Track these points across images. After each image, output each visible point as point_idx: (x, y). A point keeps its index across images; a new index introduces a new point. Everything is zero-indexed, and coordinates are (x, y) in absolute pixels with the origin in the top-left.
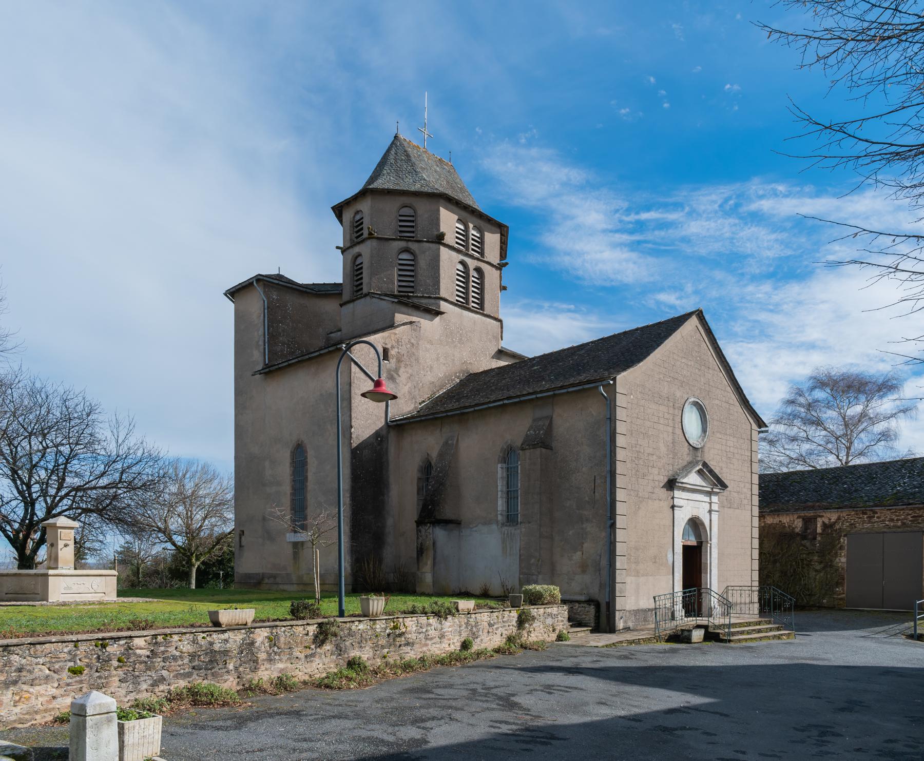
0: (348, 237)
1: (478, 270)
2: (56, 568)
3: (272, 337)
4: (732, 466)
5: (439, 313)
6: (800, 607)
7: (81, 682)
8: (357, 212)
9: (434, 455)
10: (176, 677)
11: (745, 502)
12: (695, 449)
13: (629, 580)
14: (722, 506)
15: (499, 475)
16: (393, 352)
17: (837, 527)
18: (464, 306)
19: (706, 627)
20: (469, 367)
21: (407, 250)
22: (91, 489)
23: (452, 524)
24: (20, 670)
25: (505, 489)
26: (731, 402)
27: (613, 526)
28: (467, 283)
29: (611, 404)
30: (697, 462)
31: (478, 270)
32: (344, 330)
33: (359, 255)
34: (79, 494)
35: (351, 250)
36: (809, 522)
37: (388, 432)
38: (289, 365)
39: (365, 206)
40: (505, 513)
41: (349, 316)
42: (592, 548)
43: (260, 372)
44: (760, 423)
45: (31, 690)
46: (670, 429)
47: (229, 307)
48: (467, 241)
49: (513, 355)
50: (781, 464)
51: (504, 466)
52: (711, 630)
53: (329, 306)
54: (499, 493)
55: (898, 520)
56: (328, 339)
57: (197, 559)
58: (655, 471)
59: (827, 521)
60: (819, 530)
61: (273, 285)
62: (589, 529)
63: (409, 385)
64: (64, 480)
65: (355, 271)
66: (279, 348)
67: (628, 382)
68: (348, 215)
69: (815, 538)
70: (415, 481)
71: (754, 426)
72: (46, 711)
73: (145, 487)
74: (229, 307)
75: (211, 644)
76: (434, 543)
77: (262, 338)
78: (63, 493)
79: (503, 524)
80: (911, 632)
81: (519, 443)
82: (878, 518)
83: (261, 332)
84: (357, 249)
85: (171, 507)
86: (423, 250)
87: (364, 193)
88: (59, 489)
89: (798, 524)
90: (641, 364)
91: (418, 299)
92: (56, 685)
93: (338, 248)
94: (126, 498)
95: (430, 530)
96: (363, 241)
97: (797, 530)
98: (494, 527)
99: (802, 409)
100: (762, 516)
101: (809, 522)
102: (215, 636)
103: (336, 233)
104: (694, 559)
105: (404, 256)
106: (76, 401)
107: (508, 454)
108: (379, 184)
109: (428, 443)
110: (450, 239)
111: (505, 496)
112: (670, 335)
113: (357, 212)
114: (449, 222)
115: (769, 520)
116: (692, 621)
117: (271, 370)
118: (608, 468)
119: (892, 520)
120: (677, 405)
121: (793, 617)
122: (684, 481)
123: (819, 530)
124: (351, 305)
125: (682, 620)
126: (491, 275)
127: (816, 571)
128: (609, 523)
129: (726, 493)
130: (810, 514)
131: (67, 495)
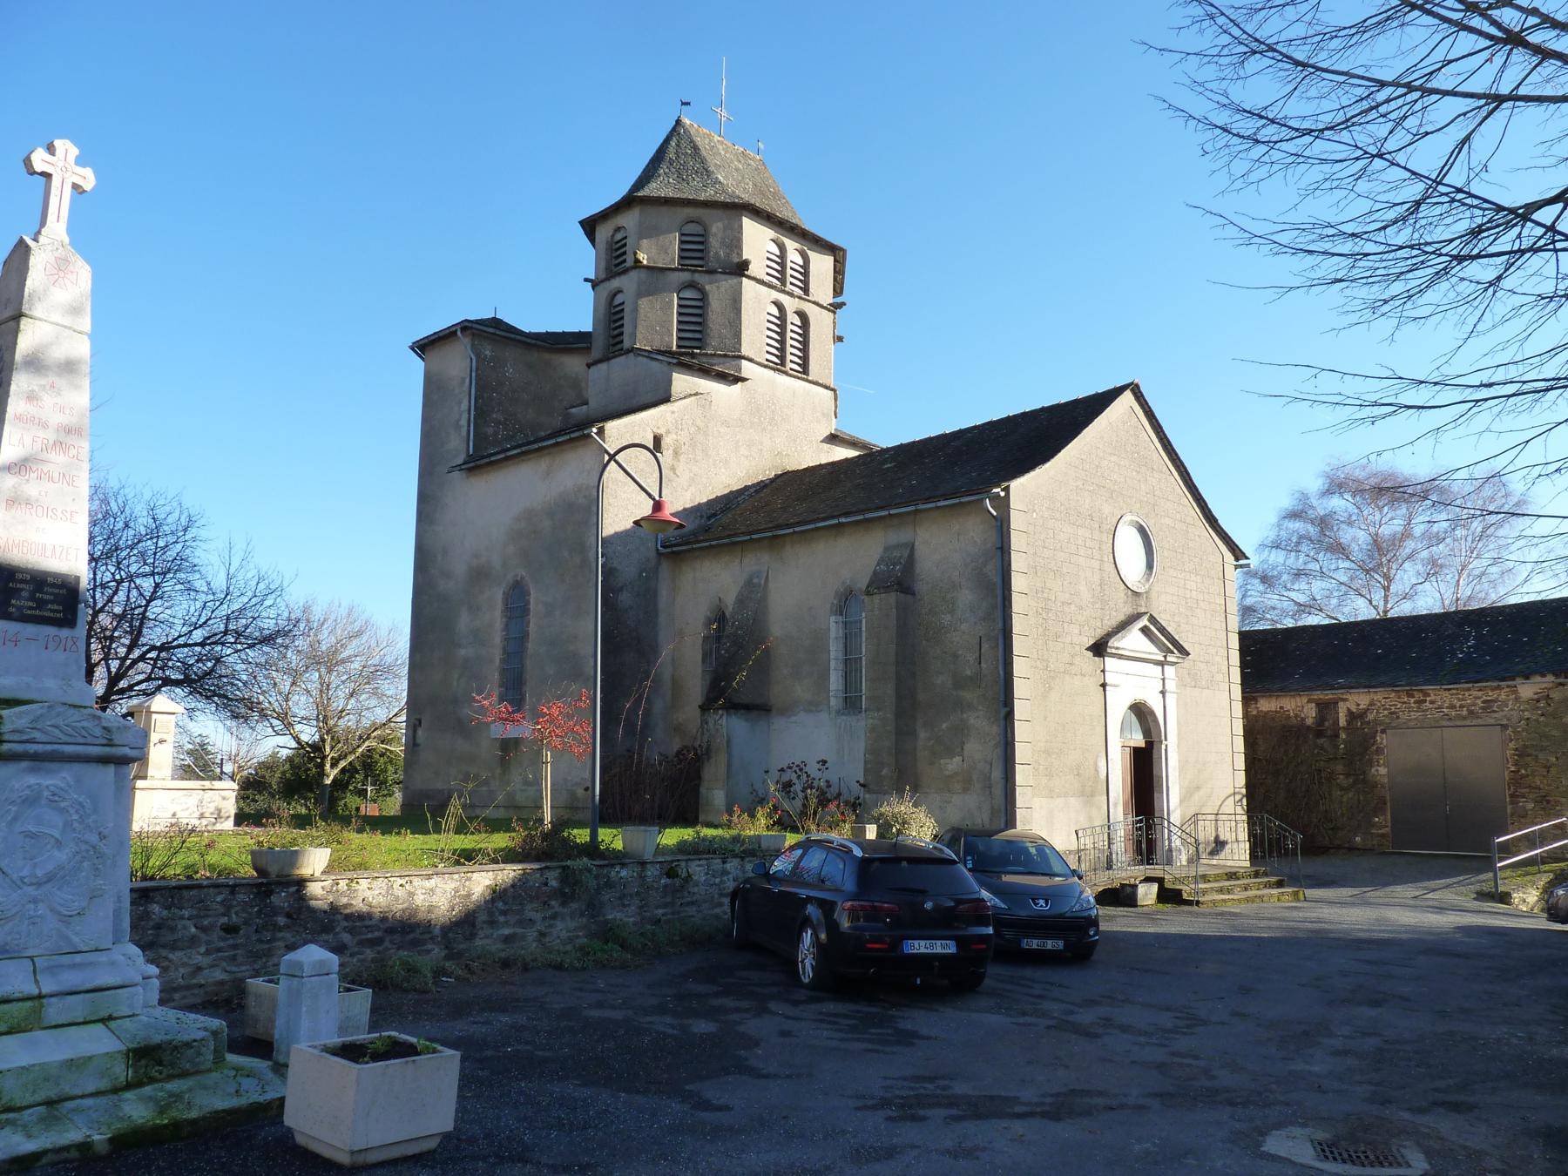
0: (603, 265)
1: (802, 315)
2: (145, 778)
3: (481, 413)
4: (1194, 620)
5: (738, 379)
6: (1312, 849)
7: (235, 947)
8: (618, 229)
9: (730, 601)
10: (361, 943)
11: (1220, 677)
12: (1136, 594)
13: (1037, 803)
14: (1182, 684)
15: (833, 634)
16: (667, 442)
17: (1371, 717)
18: (779, 365)
19: (1160, 881)
20: (786, 461)
21: (691, 285)
22: (179, 646)
23: (757, 708)
24: (158, 927)
25: (841, 656)
26: (1189, 520)
27: (1009, 716)
28: (782, 334)
29: (1002, 526)
30: (1138, 616)
31: (802, 315)
32: (593, 403)
33: (620, 291)
34: (163, 654)
35: (606, 284)
36: (1325, 708)
37: (659, 563)
38: (507, 459)
39: (629, 220)
40: (841, 695)
41: (602, 380)
42: (978, 750)
43: (459, 467)
44: (1238, 553)
45: (171, 956)
46: (1096, 564)
47: (416, 367)
48: (783, 272)
49: (852, 443)
50: (1284, 613)
51: (840, 619)
52: (1168, 885)
53: (573, 364)
54: (833, 664)
55: (1462, 706)
56: (567, 416)
57: (333, 766)
58: (1075, 629)
59: (1354, 709)
60: (1342, 722)
61: (490, 334)
62: (972, 721)
63: (693, 489)
64: (140, 633)
65: (613, 316)
66: (490, 431)
67: (1030, 494)
68: (603, 232)
69: (1337, 736)
70: (700, 641)
71: (1229, 557)
72: (188, 987)
73: (268, 640)
74: (417, 366)
75: (411, 894)
76: (729, 741)
77: (465, 416)
78: (136, 653)
79: (838, 712)
80: (1486, 888)
81: (863, 584)
82: (1432, 702)
83: (464, 406)
84: (616, 283)
85: (296, 676)
86: (717, 290)
87: (628, 202)
88: (130, 649)
89: (1310, 712)
90: (1048, 465)
91: (706, 350)
92: (202, 950)
93: (586, 280)
94: (234, 661)
95: (724, 721)
96: (625, 271)
97: (1309, 721)
98: (824, 716)
99: (1313, 530)
100: (1246, 700)
101: (1325, 708)
102: (417, 882)
103: (585, 258)
104: (1144, 765)
105: (687, 294)
106: (167, 508)
107: (845, 602)
108: (653, 189)
109: (718, 580)
110: (758, 268)
111: (841, 666)
112: (1091, 421)
113: (618, 229)
114: (757, 241)
115: (1266, 705)
116: (1141, 870)
117: (477, 463)
118: (1000, 625)
119: (1452, 707)
120: (1104, 527)
121: (1301, 864)
122: (1116, 644)
123: (1342, 722)
124: (603, 366)
125: (1127, 871)
126: (821, 323)
127: (1342, 789)
128: (1003, 711)
129: (1187, 662)
130: (1328, 695)
131: (142, 658)
